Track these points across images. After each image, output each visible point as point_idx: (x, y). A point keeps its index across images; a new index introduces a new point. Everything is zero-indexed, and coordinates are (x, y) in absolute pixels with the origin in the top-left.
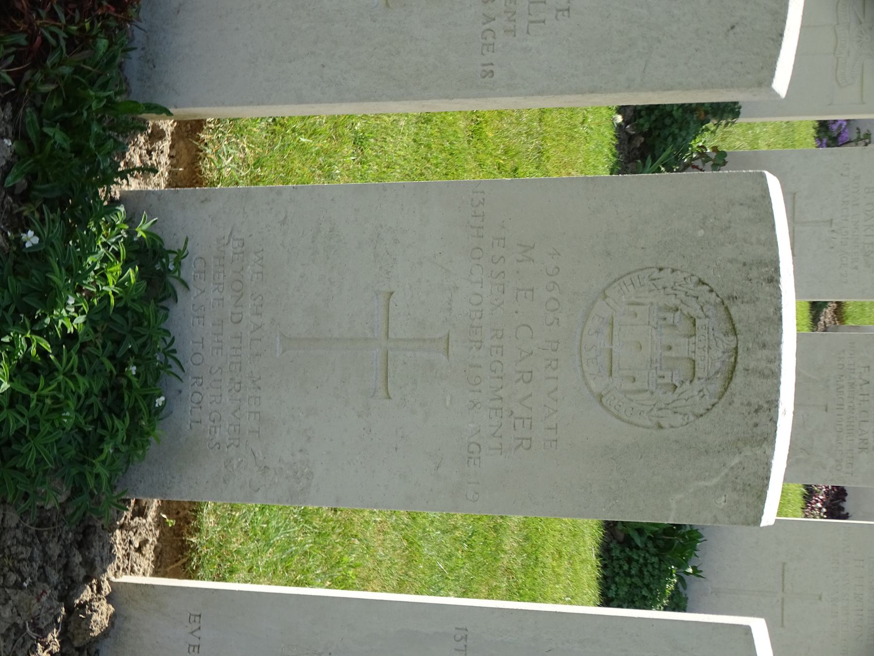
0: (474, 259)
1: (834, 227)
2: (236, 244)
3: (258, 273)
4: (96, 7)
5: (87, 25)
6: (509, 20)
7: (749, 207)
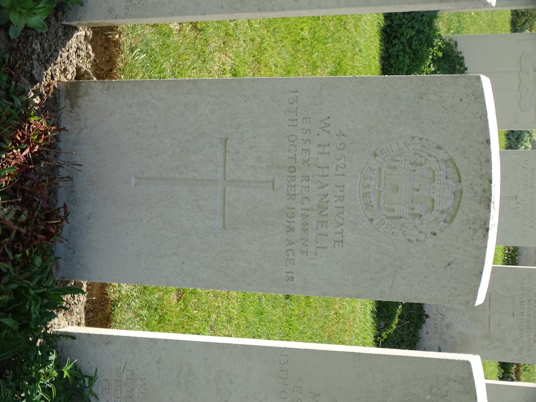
0: (282, 398)
1: (518, 201)
2: (128, 373)
3: (142, 393)
4: (33, 240)
5: (27, 252)
6: (304, 244)
7: (460, 383)
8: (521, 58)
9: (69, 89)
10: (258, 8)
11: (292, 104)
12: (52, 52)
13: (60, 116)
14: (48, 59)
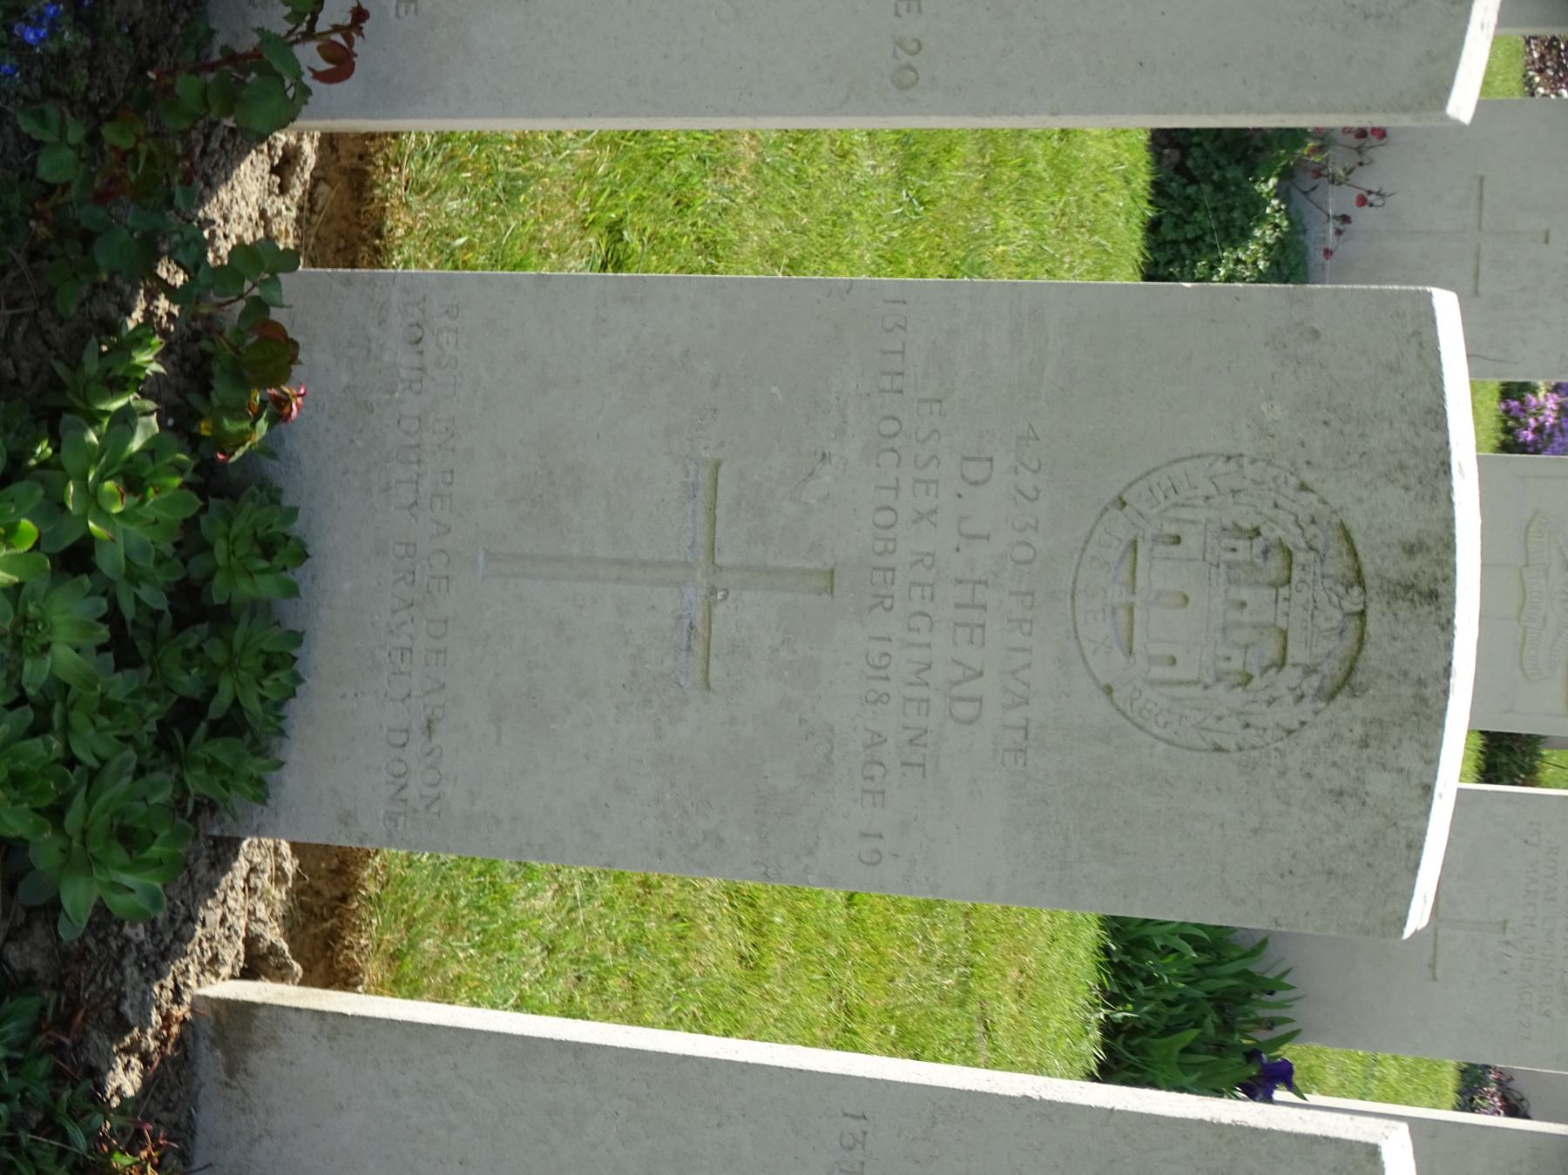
8: (1528, 527)
9: (224, 1020)
10: (763, 869)
11: (850, 1149)
12: (178, 924)
13: (197, 1093)
14: (167, 949)
